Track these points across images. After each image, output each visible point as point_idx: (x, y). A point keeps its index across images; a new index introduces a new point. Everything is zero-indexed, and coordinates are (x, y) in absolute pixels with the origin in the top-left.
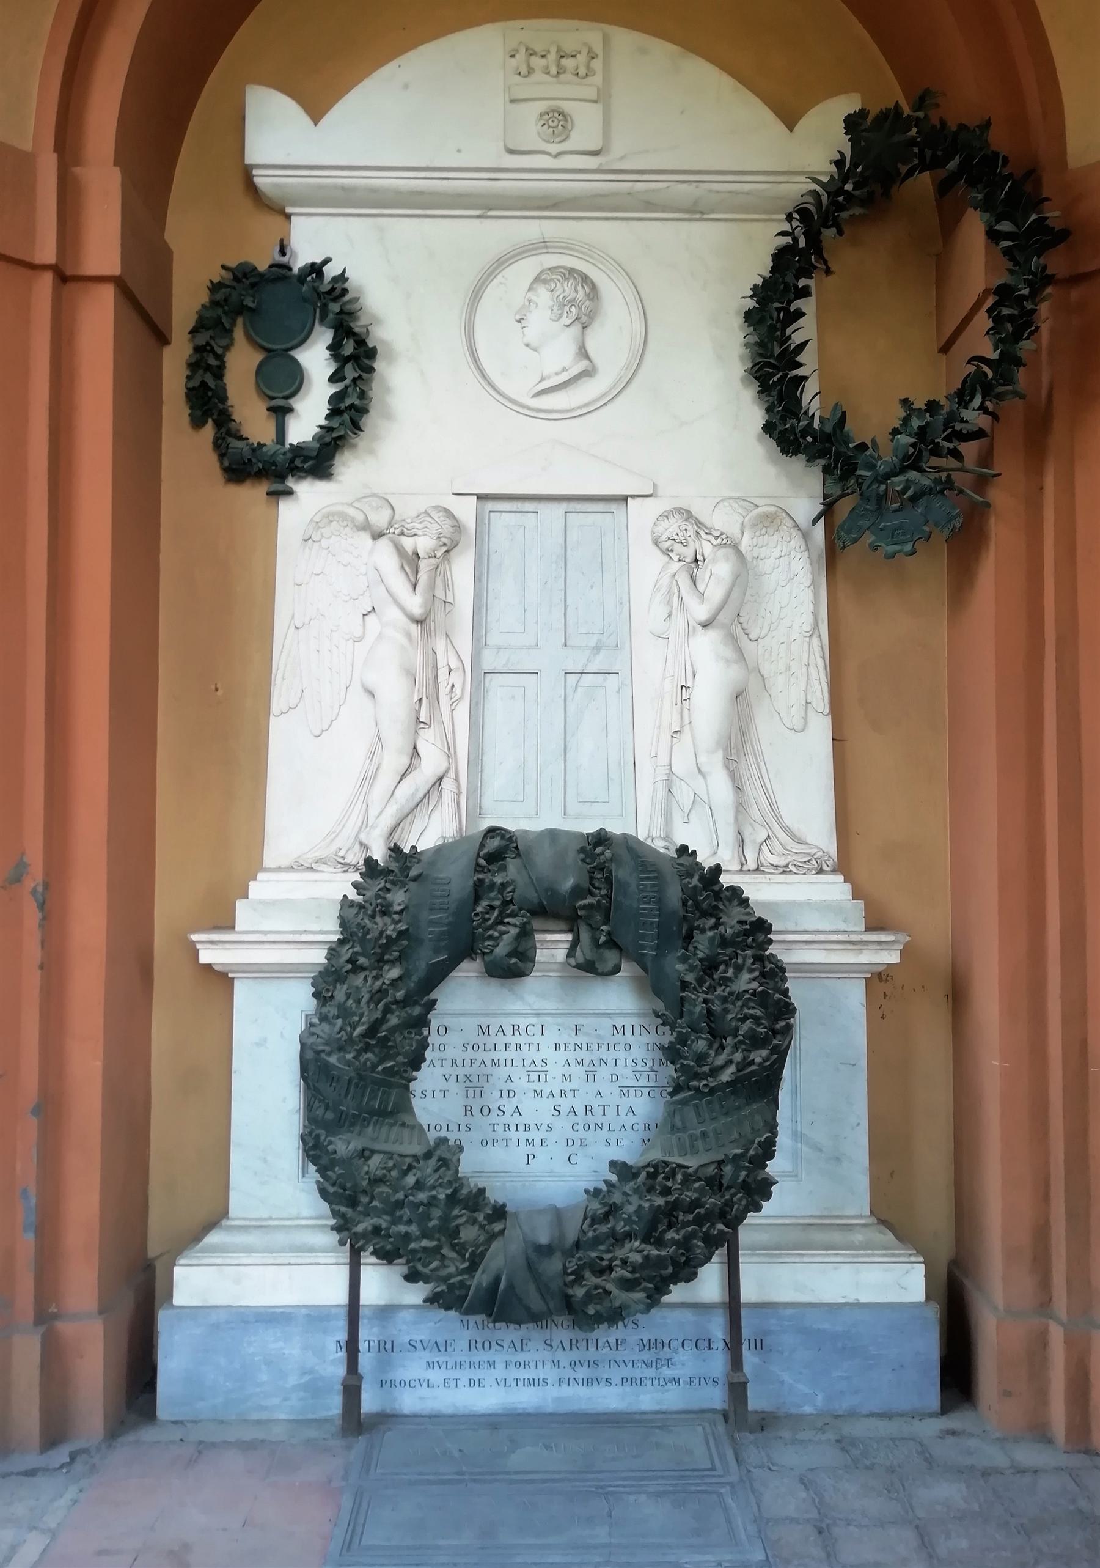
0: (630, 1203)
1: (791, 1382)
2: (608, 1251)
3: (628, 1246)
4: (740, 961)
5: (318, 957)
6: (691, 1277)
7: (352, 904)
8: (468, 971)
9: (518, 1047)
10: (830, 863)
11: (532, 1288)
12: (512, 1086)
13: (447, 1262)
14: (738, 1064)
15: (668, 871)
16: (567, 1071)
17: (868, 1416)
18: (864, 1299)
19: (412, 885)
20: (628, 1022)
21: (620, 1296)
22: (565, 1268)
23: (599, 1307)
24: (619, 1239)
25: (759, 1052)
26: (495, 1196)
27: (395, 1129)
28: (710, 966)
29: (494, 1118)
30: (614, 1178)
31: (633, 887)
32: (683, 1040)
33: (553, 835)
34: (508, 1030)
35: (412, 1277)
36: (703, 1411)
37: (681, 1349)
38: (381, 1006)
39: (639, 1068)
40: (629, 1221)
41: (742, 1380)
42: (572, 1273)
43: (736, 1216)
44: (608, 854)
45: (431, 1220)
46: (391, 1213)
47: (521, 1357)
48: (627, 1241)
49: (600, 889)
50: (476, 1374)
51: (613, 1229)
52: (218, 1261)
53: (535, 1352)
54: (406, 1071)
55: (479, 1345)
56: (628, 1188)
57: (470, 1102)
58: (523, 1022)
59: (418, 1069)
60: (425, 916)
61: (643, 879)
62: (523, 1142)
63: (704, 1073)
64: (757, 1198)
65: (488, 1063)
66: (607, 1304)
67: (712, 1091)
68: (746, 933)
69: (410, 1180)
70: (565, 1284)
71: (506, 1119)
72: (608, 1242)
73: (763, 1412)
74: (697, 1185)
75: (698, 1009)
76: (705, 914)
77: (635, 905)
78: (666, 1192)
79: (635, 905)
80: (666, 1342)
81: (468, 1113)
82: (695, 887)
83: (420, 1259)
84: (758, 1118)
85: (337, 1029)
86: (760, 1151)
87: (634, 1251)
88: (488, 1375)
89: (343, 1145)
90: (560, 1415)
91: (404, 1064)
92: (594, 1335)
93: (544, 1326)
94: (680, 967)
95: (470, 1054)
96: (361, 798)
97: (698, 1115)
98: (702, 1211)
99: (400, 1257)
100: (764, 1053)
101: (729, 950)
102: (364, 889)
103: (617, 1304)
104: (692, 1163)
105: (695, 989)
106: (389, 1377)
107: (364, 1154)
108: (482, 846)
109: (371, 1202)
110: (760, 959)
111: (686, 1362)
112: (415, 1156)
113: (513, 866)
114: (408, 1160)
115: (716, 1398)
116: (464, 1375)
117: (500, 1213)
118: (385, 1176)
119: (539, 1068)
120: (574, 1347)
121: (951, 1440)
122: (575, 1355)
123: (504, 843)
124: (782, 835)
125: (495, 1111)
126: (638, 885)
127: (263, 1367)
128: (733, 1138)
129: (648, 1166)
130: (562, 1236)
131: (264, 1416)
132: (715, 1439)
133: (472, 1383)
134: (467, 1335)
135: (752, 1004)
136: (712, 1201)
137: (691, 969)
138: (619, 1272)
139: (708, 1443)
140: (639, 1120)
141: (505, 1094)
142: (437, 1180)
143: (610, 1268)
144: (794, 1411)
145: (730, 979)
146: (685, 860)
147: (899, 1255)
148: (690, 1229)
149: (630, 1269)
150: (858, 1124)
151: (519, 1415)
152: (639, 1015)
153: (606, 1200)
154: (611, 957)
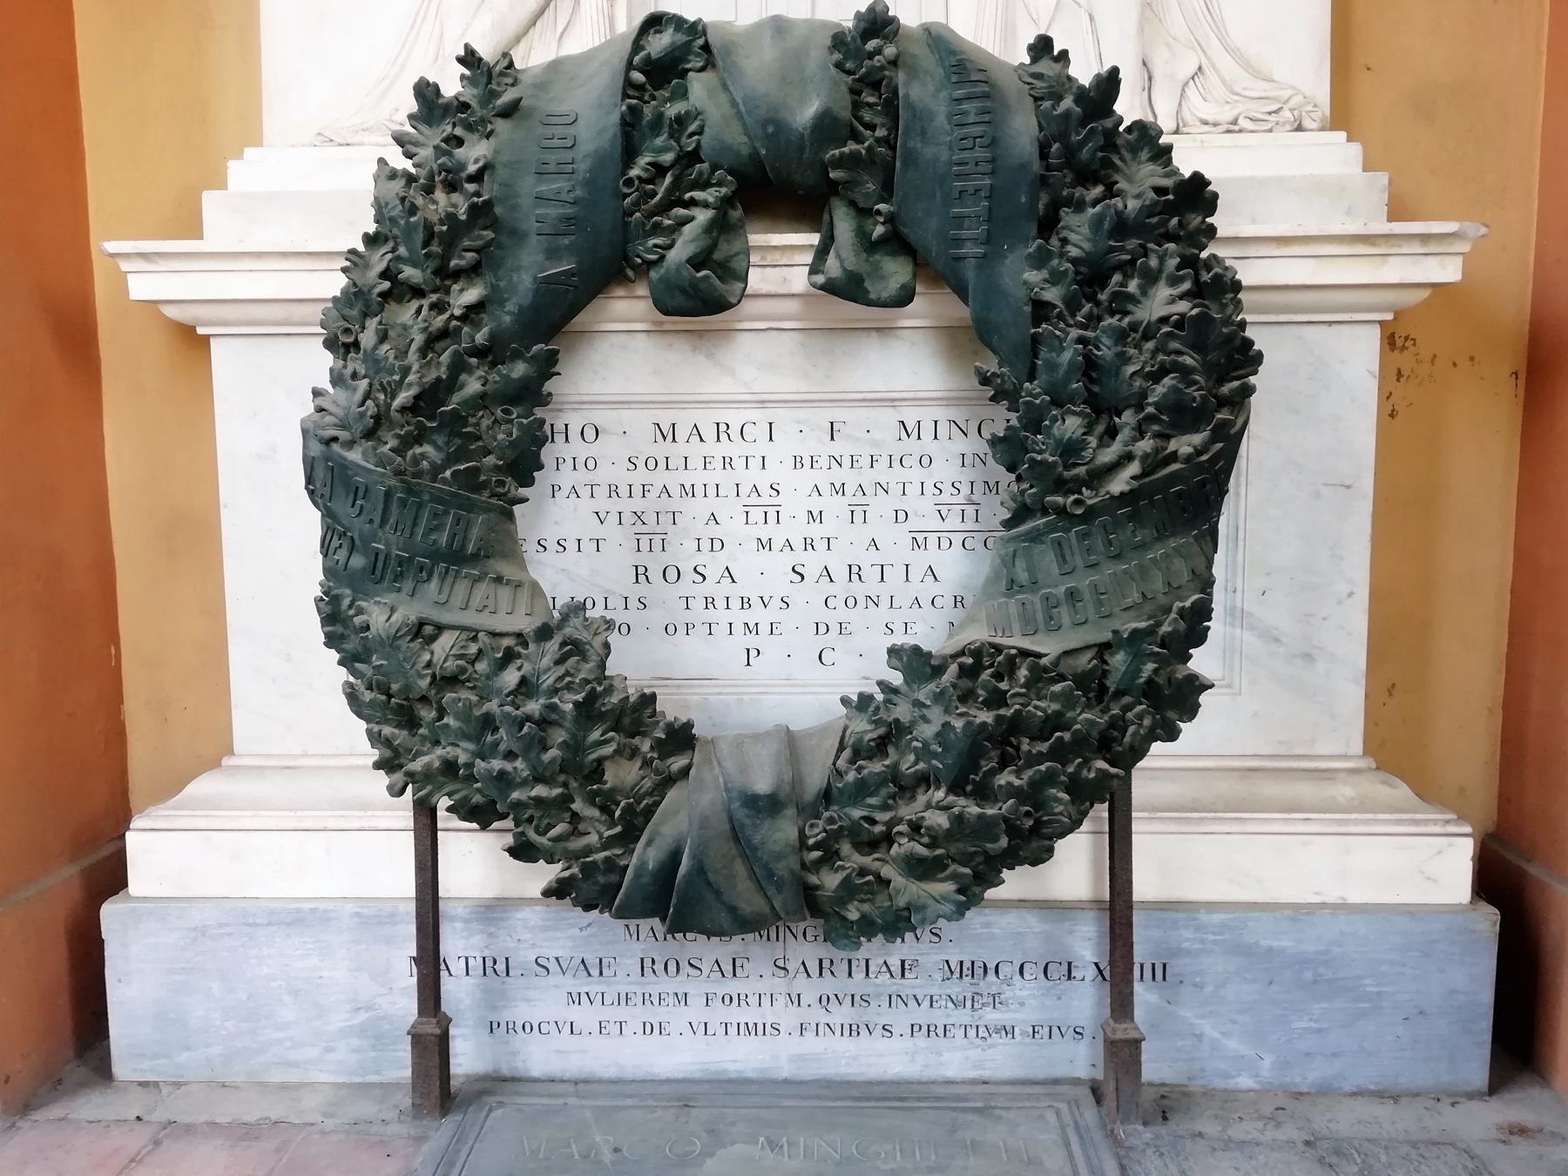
0: (926, 720)
1: (1216, 1035)
2: (885, 807)
3: (922, 799)
4: (1153, 262)
5: (334, 283)
6: (1041, 856)
7: (394, 175)
8: (627, 309)
9: (727, 462)
10: (1317, 115)
11: (740, 870)
12: (715, 531)
13: (581, 827)
14: (1145, 457)
15: (1014, 89)
16: (816, 504)
17: (1353, 1094)
18: (1354, 897)
19: (501, 125)
20: (927, 415)
21: (906, 889)
22: (802, 836)
23: (866, 907)
24: (906, 787)
25: (1186, 438)
26: (670, 708)
27: (482, 589)
28: (1091, 277)
29: (687, 586)
30: (896, 679)
31: (941, 120)
32: (1034, 422)
33: (779, 26)
34: (709, 433)
35: (522, 851)
36: (1056, 1082)
37: (1017, 977)
38: (445, 358)
39: (945, 498)
40: (924, 753)
41: (1133, 1035)
42: (816, 847)
43: (1132, 748)
44: (890, 51)
45: (545, 749)
46: (477, 738)
47: (733, 987)
48: (920, 790)
49: (872, 127)
50: (654, 1014)
51: (894, 767)
52: (202, 824)
53: (759, 978)
54: (501, 483)
55: (659, 967)
56: (924, 693)
57: (643, 558)
58: (735, 418)
59: (528, 481)
60: (528, 186)
61: (959, 101)
62: (738, 628)
63: (1076, 479)
64: (1171, 715)
65: (675, 490)
66: (882, 901)
67: (1090, 514)
68: (1169, 209)
69: (511, 677)
70: (804, 866)
71: (708, 588)
72: (884, 792)
73: (1163, 1085)
74: (1057, 688)
75: (1067, 356)
76: (1087, 177)
77: (944, 155)
78: (996, 700)
79: (944, 155)
80: (991, 966)
81: (642, 578)
82: (1067, 114)
83: (530, 820)
84: (1179, 564)
85: (359, 396)
86: (1182, 626)
87: (934, 809)
88: (677, 1017)
89: (381, 615)
90: (801, 1083)
91: (497, 468)
92: (862, 954)
93: (773, 935)
94: (1033, 276)
95: (640, 476)
96: (433, 10)
97: (1063, 559)
98: (1067, 736)
99: (503, 817)
100: (1198, 439)
101: (1132, 243)
102: (416, 144)
103: (901, 902)
104: (1048, 647)
105: (1060, 317)
106: (505, 1016)
107: (425, 632)
108: (637, 46)
109: (440, 718)
110: (1190, 262)
111: (1026, 1000)
112: (519, 635)
113: (699, 86)
114: (507, 642)
115: (1080, 1059)
116: (635, 1015)
117: (681, 738)
118: (463, 670)
119: (765, 500)
120: (826, 972)
121: (1523, 1148)
122: (828, 985)
123: (681, 38)
124: (1226, 63)
125: (688, 575)
126: (950, 116)
127: (286, 999)
128: (1129, 601)
129: (962, 653)
130: (797, 782)
131: (293, 1077)
132: (1081, 1138)
133: (648, 1029)
134: (637, 949)
135: (1175, 345)
136: (1086, 717)
137: (1055, 279)
138: (904, 846)
139: (1067, 1144)
140: (946, 589)
141: (705, 545)
142: (561, 678)
143: (888, 839)
144: (1219, 1083)
145: (1131, 298)
146: (1045, 67)
147: (1426, 822)
148: (1043, 768)
149: (926, 840)
150: (1350, 594)
151: (730, 1081)
152: (948, 402)
153: (882, 714)
154: (896, 272)
